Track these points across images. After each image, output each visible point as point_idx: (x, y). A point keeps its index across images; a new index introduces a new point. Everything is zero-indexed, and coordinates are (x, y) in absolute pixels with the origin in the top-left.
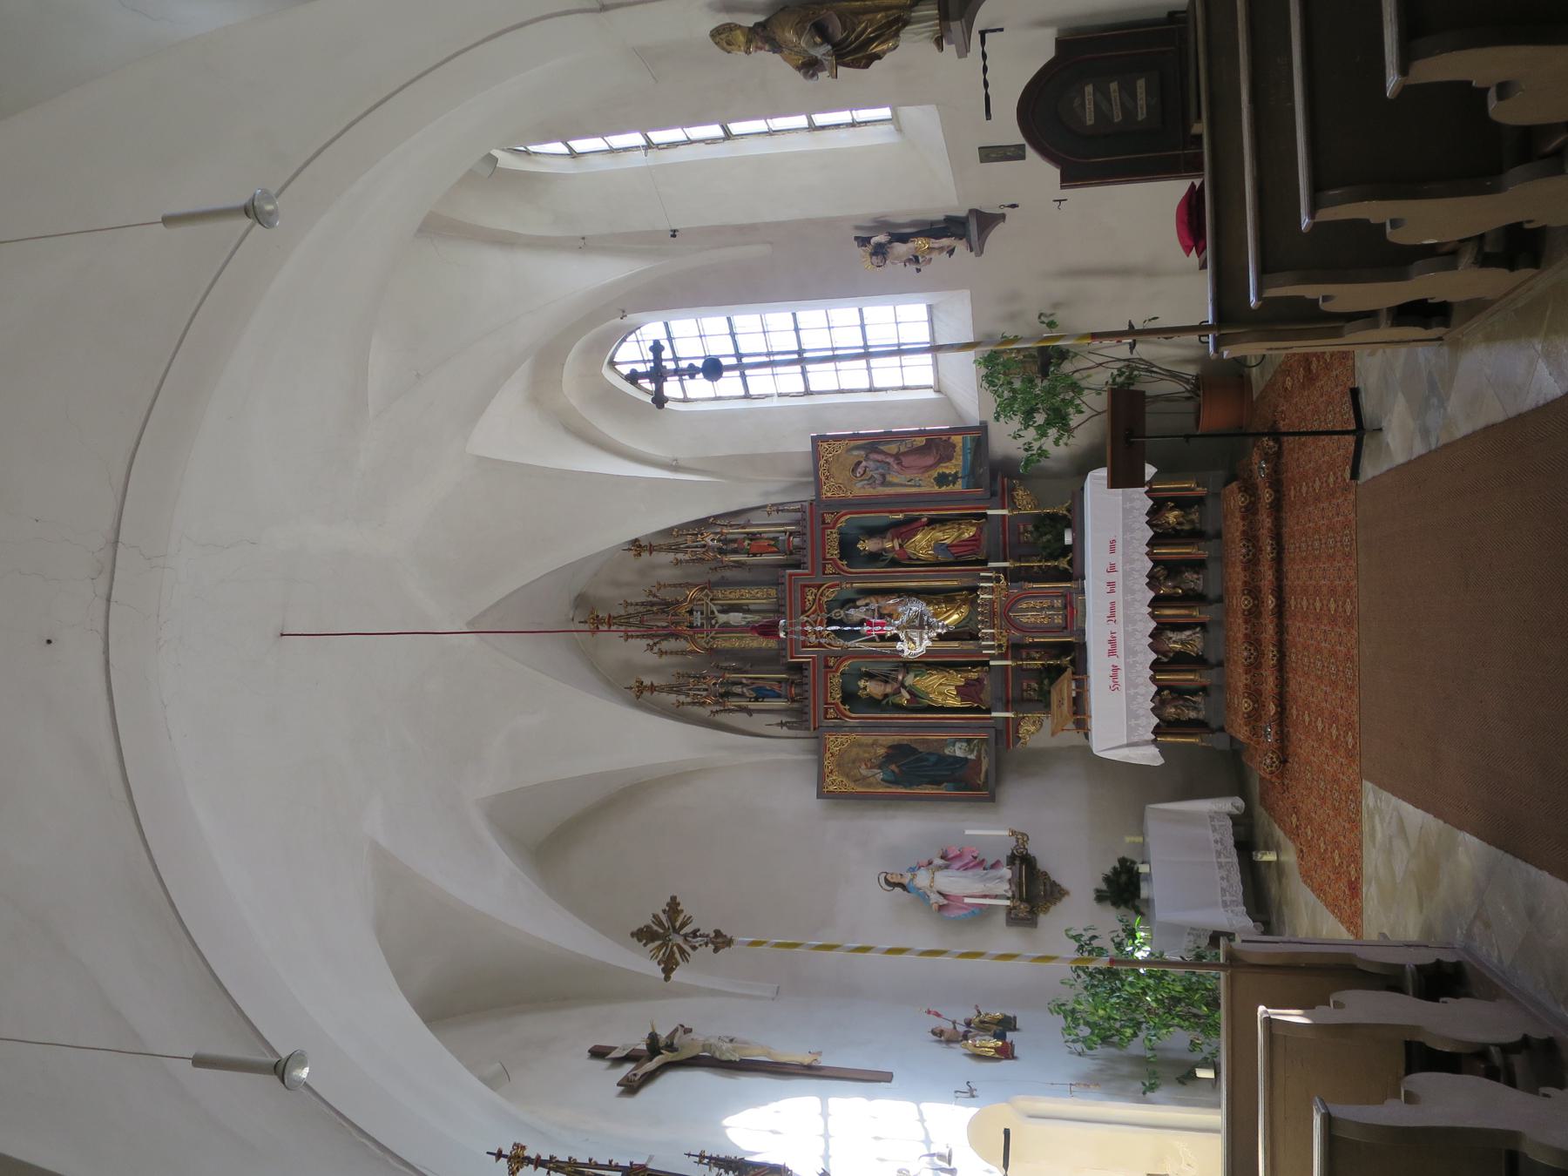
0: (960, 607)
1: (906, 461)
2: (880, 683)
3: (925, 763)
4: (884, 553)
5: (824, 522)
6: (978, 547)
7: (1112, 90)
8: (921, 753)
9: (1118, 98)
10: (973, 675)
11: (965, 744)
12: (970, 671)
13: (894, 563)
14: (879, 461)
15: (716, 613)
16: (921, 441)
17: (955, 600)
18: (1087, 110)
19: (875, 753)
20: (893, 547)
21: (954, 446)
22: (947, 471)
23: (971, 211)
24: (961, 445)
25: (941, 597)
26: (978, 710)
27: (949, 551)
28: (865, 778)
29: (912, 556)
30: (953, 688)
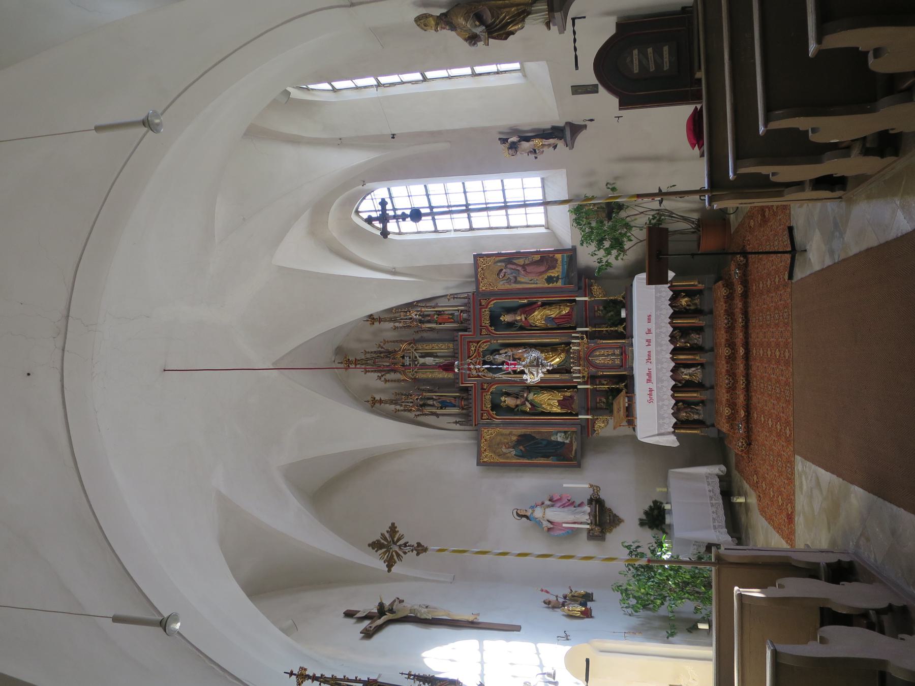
0: (560, 354)
1: (529, 269)
2: (513, 398)
3: (540, 445)
4: (516, 323)
5: (481, 305)
6: (571, 319)
7: (649, 53)
8: (537, 439)
9: (652, 57)
10: (568, 394)
11: (563, 434)
12: (566, 391)
13: (522, 328)
14: (513, 269)
15: (418, 357)
16: (537, 257)
17: (558, 350)
18: (634, 64)
19: (511, 439)
20: (521, 319)
21: (557, 260)
22: (553, 275)
23: (567, 123)
24: (561, 259)
25: (549, 348)
26: (570, 414)
27: (554, 321)
28: (505, 454)
29: (532, 324)
30: (556, 401)
